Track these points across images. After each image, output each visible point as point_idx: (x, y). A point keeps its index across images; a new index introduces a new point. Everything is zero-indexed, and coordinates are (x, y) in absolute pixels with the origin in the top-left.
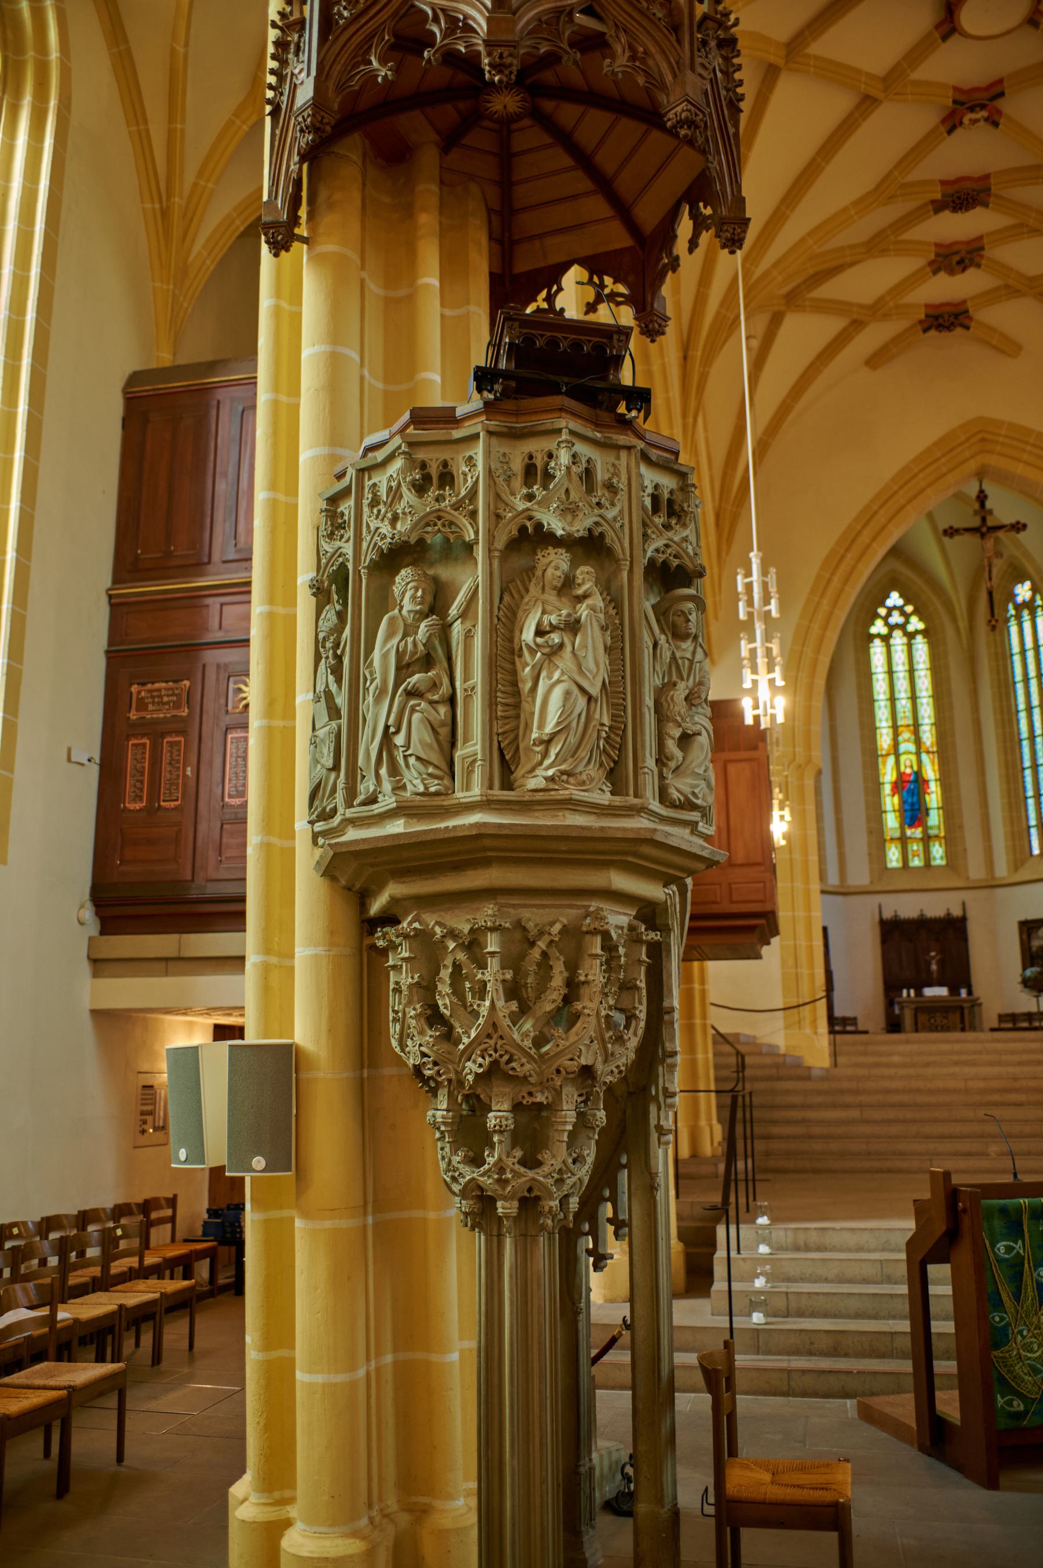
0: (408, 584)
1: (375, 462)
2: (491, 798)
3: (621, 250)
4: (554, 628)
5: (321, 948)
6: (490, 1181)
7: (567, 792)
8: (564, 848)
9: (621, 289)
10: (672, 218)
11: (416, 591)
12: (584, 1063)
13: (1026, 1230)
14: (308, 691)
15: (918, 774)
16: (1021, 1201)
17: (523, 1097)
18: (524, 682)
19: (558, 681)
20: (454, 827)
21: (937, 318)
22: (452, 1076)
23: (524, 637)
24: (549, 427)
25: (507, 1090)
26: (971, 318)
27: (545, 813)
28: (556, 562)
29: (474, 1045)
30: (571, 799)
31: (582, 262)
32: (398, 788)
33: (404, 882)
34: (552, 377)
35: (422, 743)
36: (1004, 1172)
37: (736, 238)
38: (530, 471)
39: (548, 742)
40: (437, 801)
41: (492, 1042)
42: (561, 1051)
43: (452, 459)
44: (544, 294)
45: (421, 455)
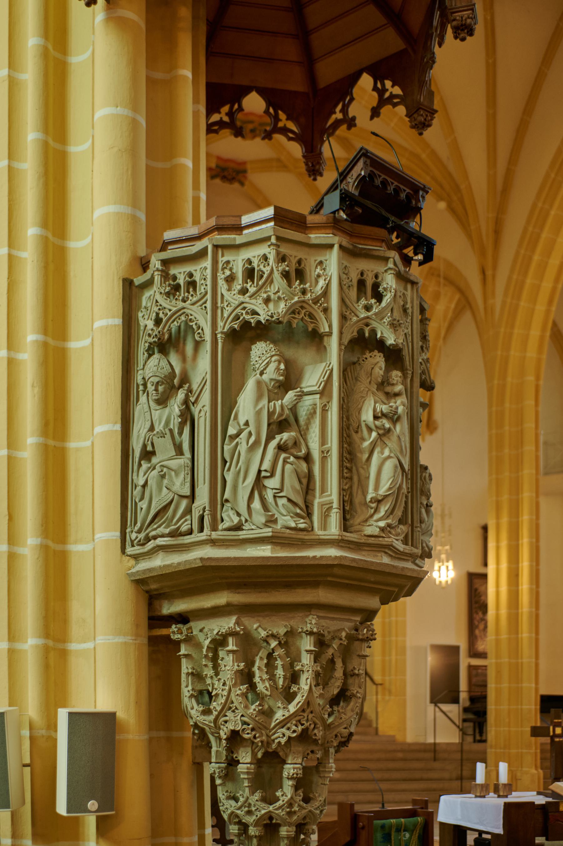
0: (272, 356)
1: (232, 243)
2: (344, 538)
3: (295, 92)
4: (384, 415)
5: (130, 638)
6: (284, 813)
7: (390, 540)
8: (372, 580)
9: (291, 125)
11: (279, 364)
12: (232, 728)
13: (393, 839)
14: (116, 423)
15: (243, 530)
16: (392, 821)
17: (308, 754)
18: (361, 452)
19: (389, 457)
20: (322, 557)
21: (224, 169)
22: (264, 738)
23: (364, 417)
24: (382, 254)
25: (301, 749)
26: (245, 177)
27: (370, 553)
28: (377, 361)
29: (292, 717)
30: (392, 545)
31: (262, 92)
32: (271, 521)
33: (239, 593)
34: (384, 213)
35: (293, 487)
36: (377, 802)
37: (427, 123)
38: (250, 273)
39: (379, 502)
40: (301, 535)
41: (305, 715)
42: (342, 722)
43: (306, 259)
44: (340, 107)
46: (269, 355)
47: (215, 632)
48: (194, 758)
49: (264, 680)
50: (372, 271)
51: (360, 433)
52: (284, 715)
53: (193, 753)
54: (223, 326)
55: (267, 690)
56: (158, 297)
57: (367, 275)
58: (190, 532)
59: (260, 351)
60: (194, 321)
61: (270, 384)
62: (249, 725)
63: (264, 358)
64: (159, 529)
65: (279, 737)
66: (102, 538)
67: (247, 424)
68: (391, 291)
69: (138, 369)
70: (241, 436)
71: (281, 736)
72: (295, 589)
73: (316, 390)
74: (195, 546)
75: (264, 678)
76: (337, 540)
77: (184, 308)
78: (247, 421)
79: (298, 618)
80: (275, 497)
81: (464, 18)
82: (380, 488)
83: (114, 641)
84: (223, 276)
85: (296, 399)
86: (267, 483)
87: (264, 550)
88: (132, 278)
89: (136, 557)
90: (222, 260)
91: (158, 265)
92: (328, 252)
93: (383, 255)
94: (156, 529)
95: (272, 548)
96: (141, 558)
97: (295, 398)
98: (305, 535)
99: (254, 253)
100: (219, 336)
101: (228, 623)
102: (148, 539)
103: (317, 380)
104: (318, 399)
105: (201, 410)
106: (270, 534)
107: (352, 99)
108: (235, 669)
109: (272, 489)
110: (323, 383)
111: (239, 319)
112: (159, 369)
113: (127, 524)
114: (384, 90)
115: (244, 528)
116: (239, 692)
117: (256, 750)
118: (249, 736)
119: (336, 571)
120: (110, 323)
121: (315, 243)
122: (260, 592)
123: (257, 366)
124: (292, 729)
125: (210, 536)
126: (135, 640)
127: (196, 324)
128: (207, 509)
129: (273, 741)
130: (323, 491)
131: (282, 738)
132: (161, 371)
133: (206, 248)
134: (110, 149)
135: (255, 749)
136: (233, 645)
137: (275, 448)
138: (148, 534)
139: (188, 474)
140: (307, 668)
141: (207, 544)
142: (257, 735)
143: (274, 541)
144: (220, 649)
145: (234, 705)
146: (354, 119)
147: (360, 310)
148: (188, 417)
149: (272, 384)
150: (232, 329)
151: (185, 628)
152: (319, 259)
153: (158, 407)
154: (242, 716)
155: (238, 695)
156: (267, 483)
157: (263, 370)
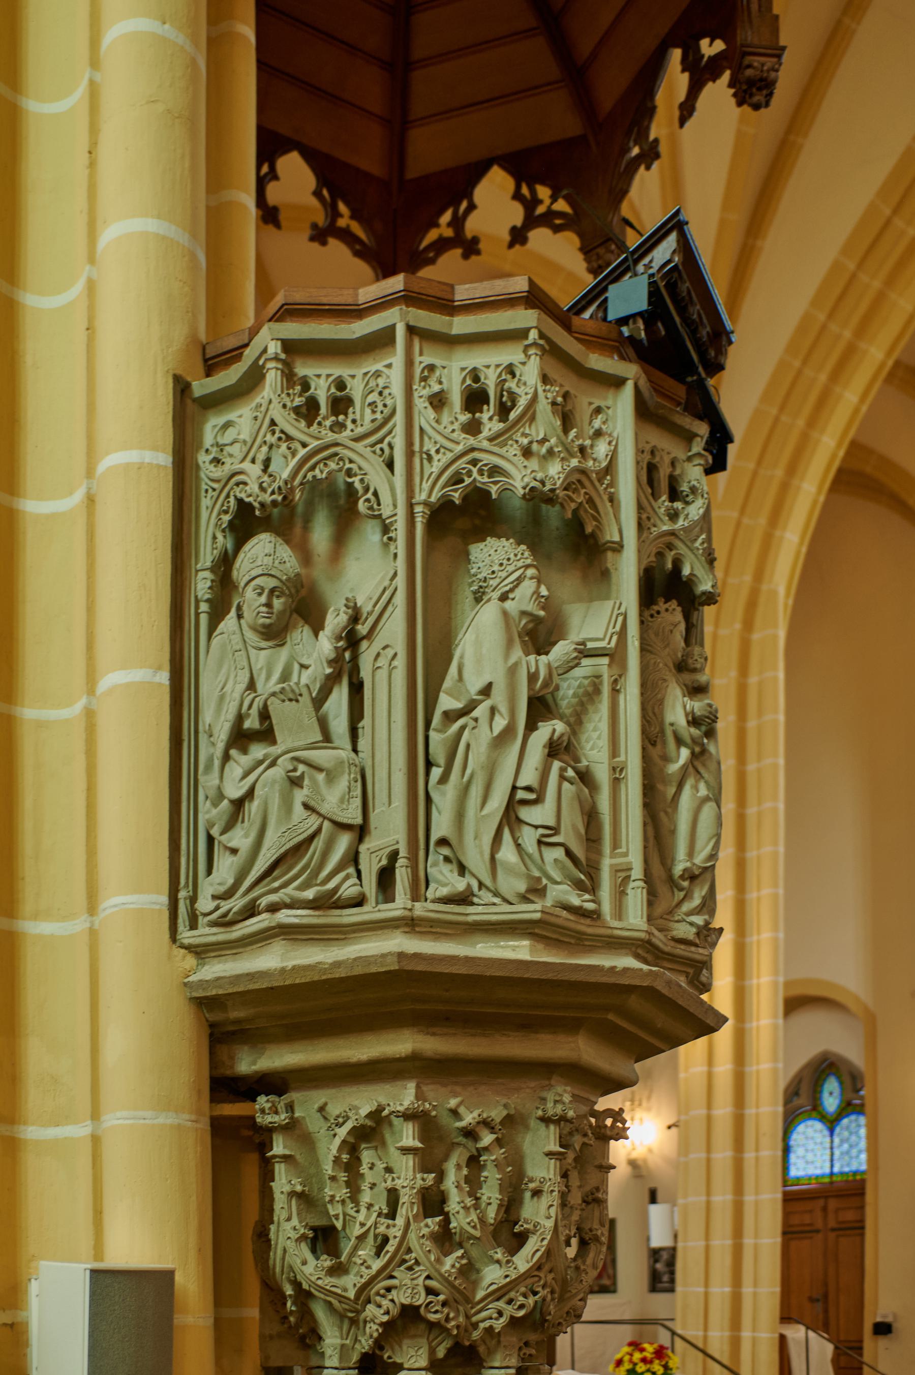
5: (187, 1116)
9: (357, 229)
10: (650, 73)
12: (407, 1301)
23: (669, 717)
25: (514, 1339)
31: (311, 157)
33: (434, 1034)
38: (475, 399)
40: (584, 926)
41: (542, 1275)
44: (446, 217)
45: (302, 370)
46: (520, 564)
47: (364, 1112)
48: (266, 1357)
49: (469, 1208)
50: (668, 453)
51: (659, 746)
52: (507, 1276)
53: (263, 1349)
54: (428, 492)
55: (474, 1227)
56: (276, 412)
57: (661, 457)
58: (359, 902)
59: (494, 555)
60: (356, 475)
61: (520, 621)
62: (437, 1295)
63: (511, 568)
64: (282, 891)
65: (491, 1318)
66: (127, 906)
67: (486, 691)
68: (702, 496)
69: (199, 566)
70: (475, 714)
71: (495, 1315)
72: (536, 1033)
73: (604, 648)
74: (362, 931)
75: (469, 1205)
76: (642, 940)
77: (337, 444)
78: (490, 685)
79: (528, 1091)
80: (540, 842)
81: (765, 68)
82: (696, 854)
83: (155, 1121)
84: (426, 392)
85: (576, 658)
86: (525, 813)
87: (514, 948)
88: (189, 379)
89: (200, 952)
90: (422, 360)
91: (274, 348)
92: (611, 393)
93: (687, 427)
94: (276, 890)
95: (530, 945)
96: (213, 954)
97: (575, 654)
98: (589, 926)
99: (489, 361)
100: (418, 509)
101: (405, 1096)
102: (251, 911)
103: (604, 630)
104: (606, 667)
105: (378, 655)
106: (538, 916)
107: (472, 207)
108: (417, 1186)
109: (536, 827)
110: (615, 638)
111: (462, 481)
112: (277, 562)
113: (179, 883)
114: (537, 202)
115: (476, 900)
116: (425, 1231)
117: (433, 1344)
118: (438, 1316)
119: (634, 1003)
120: (147, 460)
121: (596, 368)
122: (473, 1035)
123: (494, 583)
124: (519, 1303)
125: (410, 910)
126: (196, 1121)
127: (362, 481)
128: (401, 855)
129: (475, 1326)
130: (616, 845)
131: (497, 1319)
132: (281, 567)
133: (393, 328)
134: (148, 102)
135: (433, 1340)
136: (414, 1139)
137: (544, 747)
138: (255, 900)
139: (356, 781)
140: (550, 1186)
141: (397, 927)
142: (452, 1315)
143: (536, 931)
144: (363, 1146)
145: (413, 1255)
146: (475, 240)
147: (662, 517)
148: (346, 670)
149: (523, 622)
150: (445, 499)
151: (282, 1104)
152: (597, 403)
153: (264, 644)
154: (428, 1277)
155: (424, 1236)
156: (525, 813)
157: (507, 592)
